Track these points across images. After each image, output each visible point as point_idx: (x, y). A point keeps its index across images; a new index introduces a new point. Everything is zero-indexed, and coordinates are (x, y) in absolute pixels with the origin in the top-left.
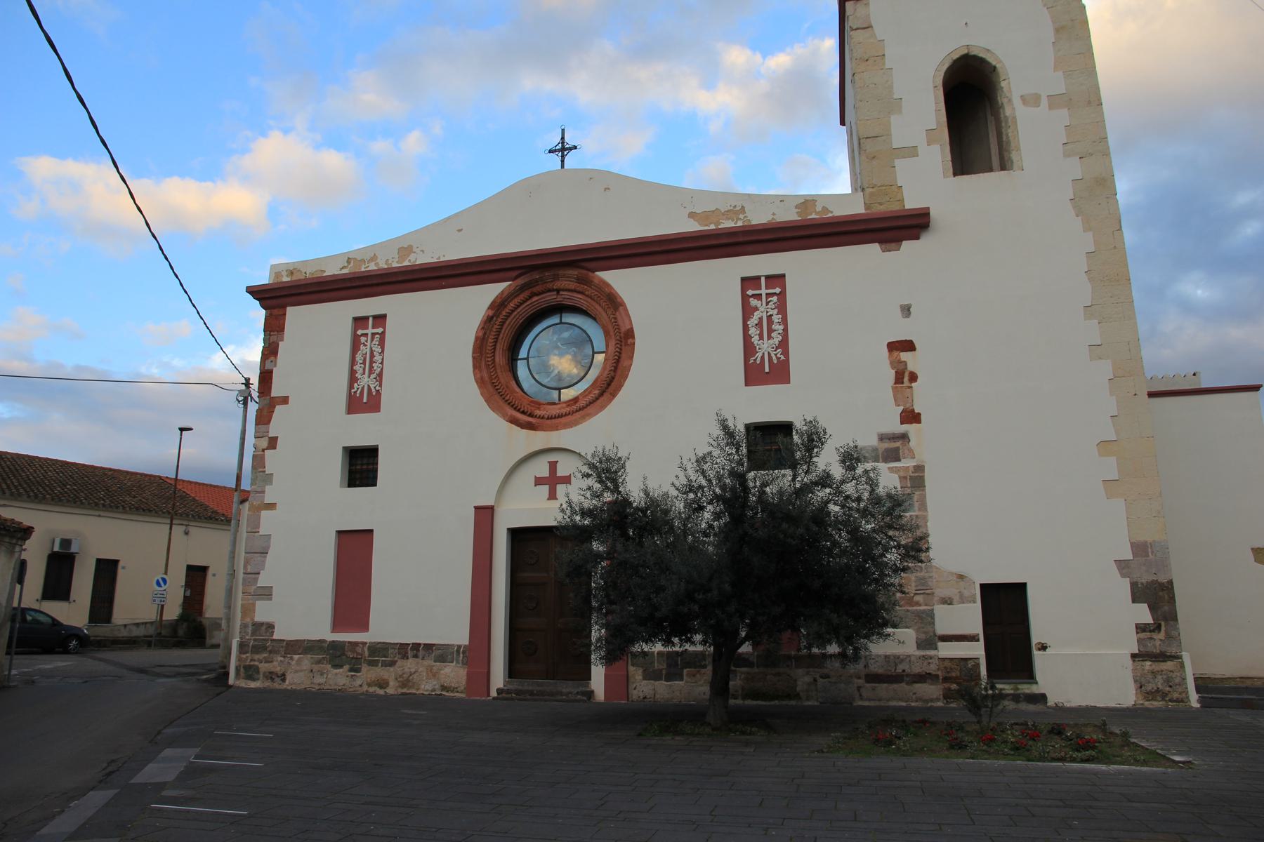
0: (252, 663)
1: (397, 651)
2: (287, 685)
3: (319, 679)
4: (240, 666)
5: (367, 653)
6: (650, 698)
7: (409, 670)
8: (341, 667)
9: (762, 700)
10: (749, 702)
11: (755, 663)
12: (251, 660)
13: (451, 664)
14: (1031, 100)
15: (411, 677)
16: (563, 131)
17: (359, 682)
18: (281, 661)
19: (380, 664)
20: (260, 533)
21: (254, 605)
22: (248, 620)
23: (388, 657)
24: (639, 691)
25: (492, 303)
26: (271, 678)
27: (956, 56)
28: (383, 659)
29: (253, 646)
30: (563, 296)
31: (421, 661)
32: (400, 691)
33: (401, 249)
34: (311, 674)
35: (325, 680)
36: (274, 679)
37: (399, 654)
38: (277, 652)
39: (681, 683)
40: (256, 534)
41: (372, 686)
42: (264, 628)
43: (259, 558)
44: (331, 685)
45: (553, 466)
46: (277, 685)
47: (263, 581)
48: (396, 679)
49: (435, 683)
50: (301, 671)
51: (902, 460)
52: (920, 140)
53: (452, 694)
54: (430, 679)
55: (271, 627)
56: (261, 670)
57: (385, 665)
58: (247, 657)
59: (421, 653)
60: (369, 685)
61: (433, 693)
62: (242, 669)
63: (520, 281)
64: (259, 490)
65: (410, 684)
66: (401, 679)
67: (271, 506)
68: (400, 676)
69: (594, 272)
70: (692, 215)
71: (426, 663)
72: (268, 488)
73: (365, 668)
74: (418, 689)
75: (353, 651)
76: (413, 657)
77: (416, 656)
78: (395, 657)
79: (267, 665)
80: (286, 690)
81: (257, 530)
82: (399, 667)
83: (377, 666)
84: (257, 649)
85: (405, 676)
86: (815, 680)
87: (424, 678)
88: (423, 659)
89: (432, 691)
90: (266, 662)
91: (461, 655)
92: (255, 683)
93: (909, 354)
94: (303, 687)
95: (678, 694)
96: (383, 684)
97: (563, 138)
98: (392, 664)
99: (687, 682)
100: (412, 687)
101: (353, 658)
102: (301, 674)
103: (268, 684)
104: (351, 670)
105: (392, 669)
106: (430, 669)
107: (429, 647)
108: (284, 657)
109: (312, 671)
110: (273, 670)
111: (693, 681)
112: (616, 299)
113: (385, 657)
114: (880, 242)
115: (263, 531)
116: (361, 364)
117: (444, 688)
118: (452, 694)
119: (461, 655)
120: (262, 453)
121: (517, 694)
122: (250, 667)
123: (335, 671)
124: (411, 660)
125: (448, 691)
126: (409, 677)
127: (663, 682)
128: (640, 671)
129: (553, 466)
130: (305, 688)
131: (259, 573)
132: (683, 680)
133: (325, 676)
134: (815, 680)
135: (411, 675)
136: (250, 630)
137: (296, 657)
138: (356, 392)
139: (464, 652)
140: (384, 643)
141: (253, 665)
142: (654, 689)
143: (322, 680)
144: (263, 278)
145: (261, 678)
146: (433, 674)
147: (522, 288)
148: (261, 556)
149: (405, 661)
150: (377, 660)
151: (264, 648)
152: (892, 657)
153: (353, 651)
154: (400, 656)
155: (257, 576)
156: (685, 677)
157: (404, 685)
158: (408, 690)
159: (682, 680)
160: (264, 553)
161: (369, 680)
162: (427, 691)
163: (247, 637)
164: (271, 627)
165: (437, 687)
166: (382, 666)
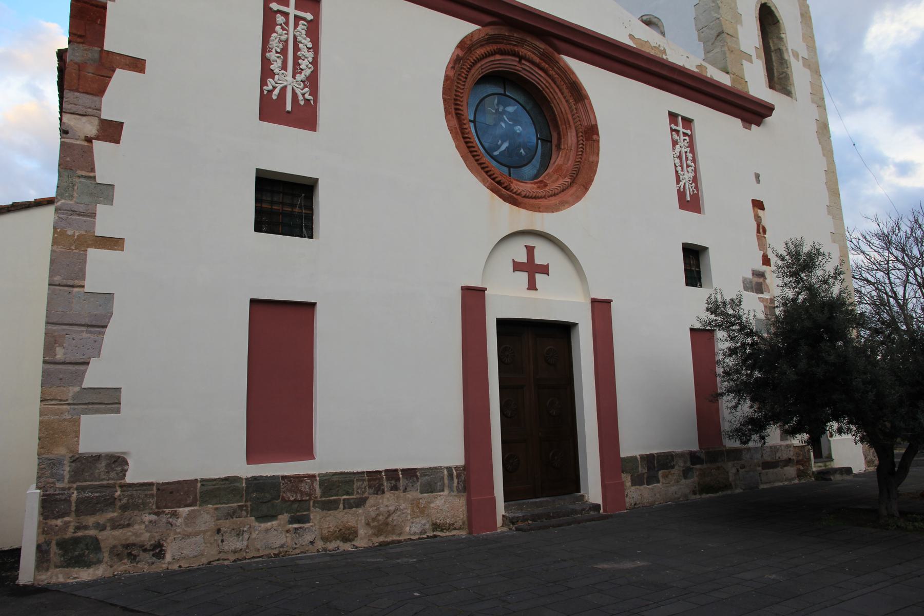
0: (80, 534)
1: (366, 483)
2: (169, 563)
3: (233, 544)
4: (48, 544)
5: (318, 492)
6: (639, 504)
7: (386, 509)
8: (273, 517)
9: (712, 493)
10: (704, 496)
11: (704, 459)
12: (78, 528)
13: (442, 493)
15: (390, 519)
17: (308, 537)
18: (151, 522)
19: (341, 506)
20: (86, 290)
21: (76, 423)
22: (61, 451)
23: (352, 494)
24: (630, 498)
25: (460, 42)
26: (130, 554)
27: (773, 9)
28: (345, 497)
29: (80, 502)
30: (523, 66)
31: (402, 494)
32: (377, 540)
34: (218, 537)
35: (245, 543)
36: (135, 556)
37: (370, 487)
38: (140, 507)
39: (659, 485)
40: (76, 290)
41: (331, 542)
42: (103, 464)
43: (85, 335)
44: (258, 550)
45: (530, 250)
46: (146, 566)
47: (95, 376)
48: (368, 524)
49: (423, 522)
50: (197, 534)
51: (765, 293)
53: (448, 534)
54: (418, 517)
55: (118, 462)
56: (102, 545)
57: (349, 505)
58: (67, 523)
59: (402, 483)
60: (325, 539)
61: (425, 536)
62: (54, 548)
63: (490, 31)
64: (81, 208)
65: (389, 528)
66: (375, 523)
67: (114, 243)
68: (374, 519)
69: (559, 53)
70: (631, 37)
71: (411, 495)
72: (101, 209)
73: (316, 515)
74: (400, 534)
75: (296, 490)
76: (391, 490)
77: (395, 488)
78: (364, 492)
79: (116, 533)
80: (169, 574)
81: (81, 283)
82: (371, 506)
83: (337, 508)
84: (87, 507)
85: (381, 518)
86: (738, 471)
87: (409, 517)
88: (405, 490)
89: (421, 533)
90: (114, 528)
91: (456, 480)
92: (91, 570)
93: (762, 211)
94: (204, 560)
95: (659, 497)
96: (348, 535)
98: (361, 503)
99: (663, 483)
100: (393, 532)
101: (295, 500)
102: (199, 539)
103: (123, 567)
104: (293, 520)
105: (360, 511)
106: (415, 503)
107: (410, 473)
108: (157, 514)
109: (219, 531)
110: (132, 539)
111: (667, 482)
112: (582, 90)
113: (348, 494)
114: (743, 120)
115: (92, 284)
116: (277, 52)
117: (436, 526)
118: (448, 534)
119: (456, 480)
120: (86, 144)
121: (533, 520)
122: (76, 541)
123: (264, 526)
124: (388, 495)
125: (442, 530)
126: (387, 518)
127: (645, 486)
128: (629, 478)
129: (530, 250)
130: (209, 563)
131: (88, 363)
132: (659, 483)
133: (246, 536)
134: (738, 471)
135: (389, 515)
136: (66, 470)
137: (184, 511)
138: (270, 92)
139: (458, 476)
140: (341, 473)
141: (85, 537)
142: (641, 494)
143: (240, 544)
145: (105, 560)
146: (420, 510)
147: (490, 40)
148: (87, 332)
149: (379, 497)
150: (335, 500)
151: (110, 502)
152: (773, 448)
153: (296, 490)
154: (371, 491)
155: (82, 368)
156: (661, 479)
157: (379, 531)
158: (386, 537)
159: (658, 482)
160: (99, 325)
161: (325, 532)
162: (415, 533)
163: (59, 485)
164: (118, 462)
165: (427, 526)
166: (344, 508)
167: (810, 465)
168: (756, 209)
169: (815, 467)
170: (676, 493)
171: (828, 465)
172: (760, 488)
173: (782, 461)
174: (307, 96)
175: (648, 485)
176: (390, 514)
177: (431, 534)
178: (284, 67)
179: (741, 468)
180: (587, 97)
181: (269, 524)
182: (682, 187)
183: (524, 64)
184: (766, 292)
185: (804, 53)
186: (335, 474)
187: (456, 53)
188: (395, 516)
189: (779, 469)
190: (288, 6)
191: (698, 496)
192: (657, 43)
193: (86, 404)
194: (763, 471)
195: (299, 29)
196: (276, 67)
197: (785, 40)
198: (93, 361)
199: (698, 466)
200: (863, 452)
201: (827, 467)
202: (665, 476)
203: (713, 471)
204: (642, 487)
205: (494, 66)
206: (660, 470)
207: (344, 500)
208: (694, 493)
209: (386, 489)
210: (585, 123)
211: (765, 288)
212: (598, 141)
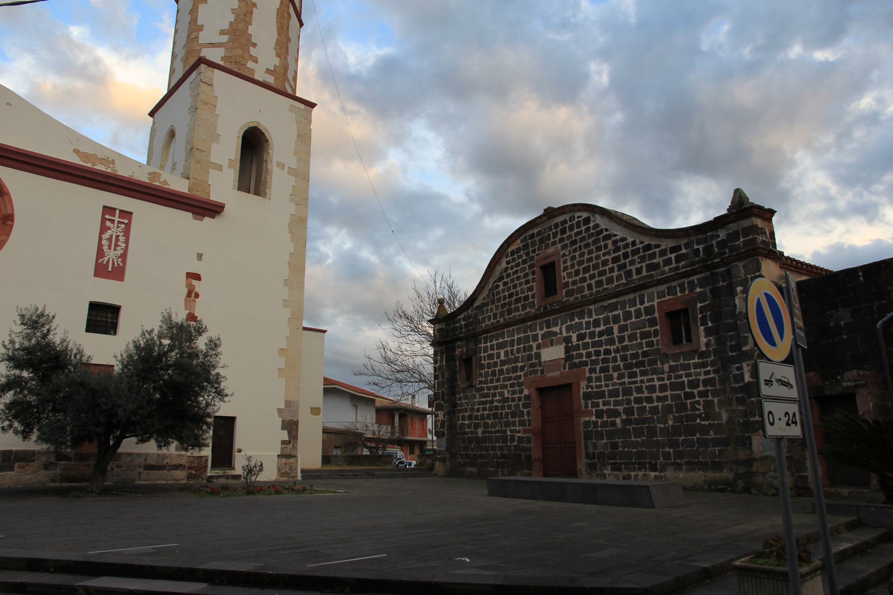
114: (193, 213)
168: (190, 279)
172: (136, 483)
173: (169, 466)
178: (110, 248)
179: (117, 467)
180: (8, 194)
182: (105, 261)
185: (292, 162)
189: (166, 471)
192: (105, 156)
194: (145, 471)
196: (105, 248)
197: (270, 155)
202: (19, 467)
203: (81, 467)
206: (17, 462)
210: (3, 213)
212: (12, 226)
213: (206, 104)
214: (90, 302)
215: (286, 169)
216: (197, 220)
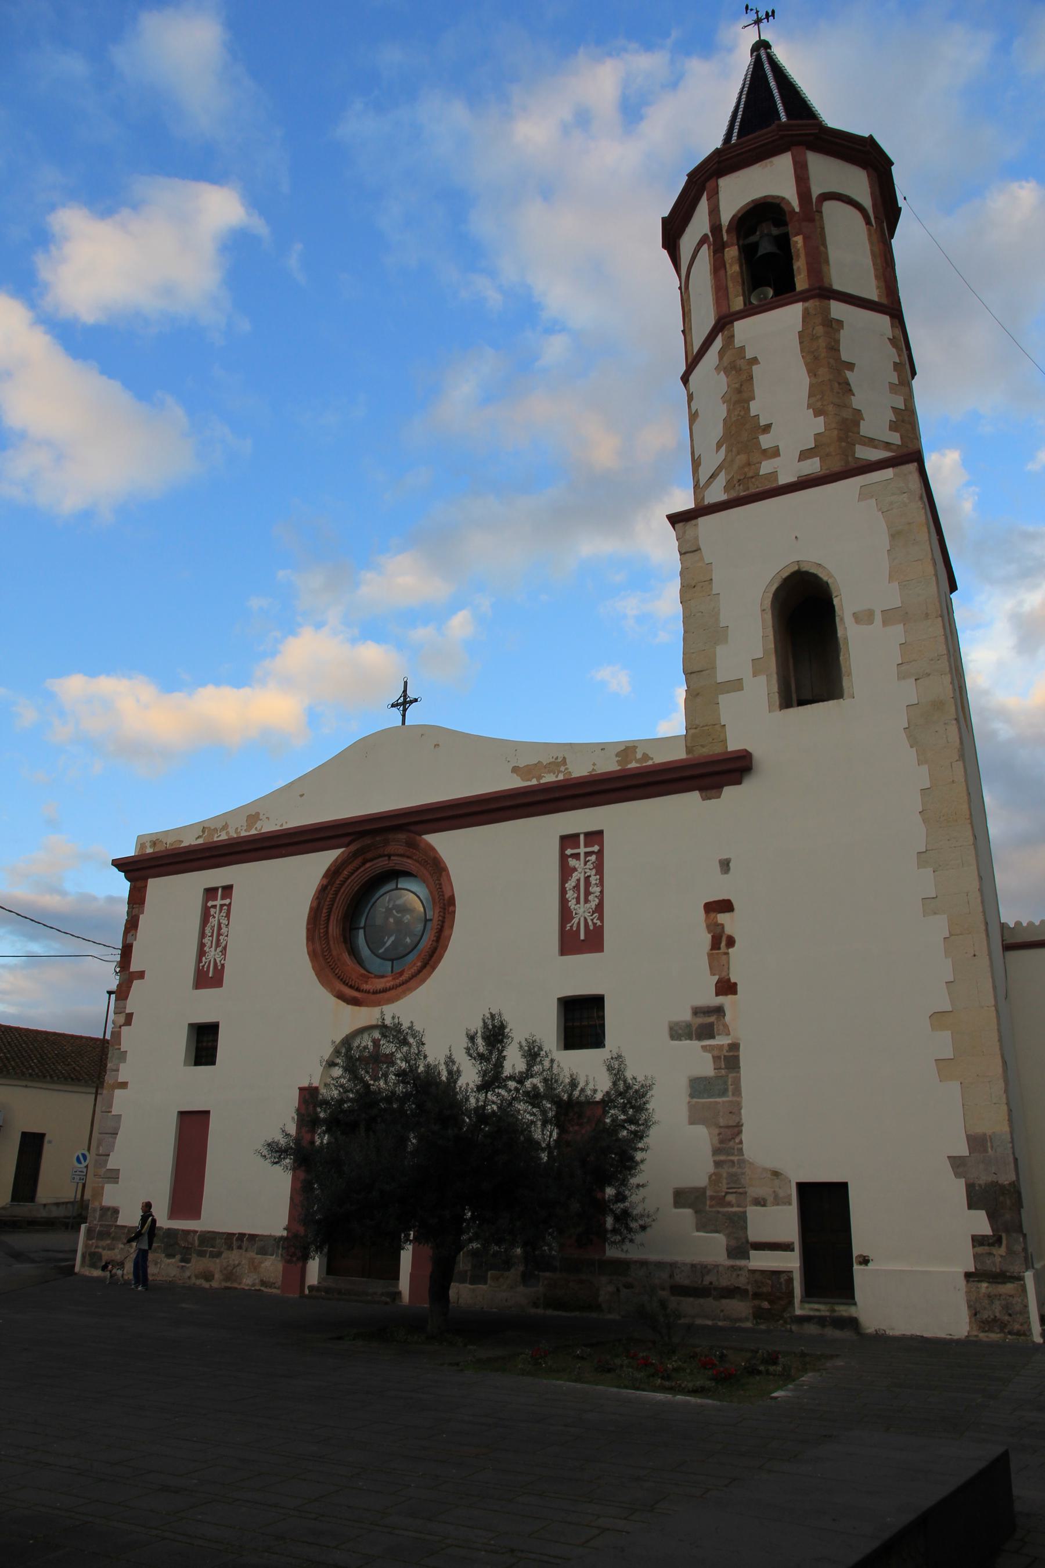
5: (197, 1243)
10: (550, 1312)
14: (864, 617)
15: (234, 1271)
16: (406, 683)
17: (188, 1274)
19: (208, 1255)
20: (113, 1113)
28: (211, 1249)
30: (394, 862)
31: (244, 1253)
32: (224, 1284)
33: (249, 817)
49: (255, 1277)
52: (746, 673)
59: (245, 1243)
60: (197, 1277)
62: (87, 1256)
63: (353, 847)
69: (420, 835)
77: (240, 1247)
79: (109, 1252)
86: (618, 1290)
88: (246, 1251)
96: (208, 1276)
97: (405, 691)
98: (218, 1255)
101: (184, 1247)
104: (182, 1260)
107: (253, 1237)
114: (701, 789)
117: (263, 1283)
124: (235, 1252)
125: (266, 1287)
131: (109, 1155)
134: (618, 1290)
135: (234, 1268)
144: (129, 851)
146: (254, 1267)
147: (355, 855)
151: (108, 1234)
159: (485, 1283)
162: (248, 1285)
164: (115, 1211)
165: (257, 1281)
166: (209, 1257)
167: (791, 1303)
169: (801, 1309)
170: (506, 1300)
171: (828, 1311)
173: (715, 1289)
174: (595, 921)
175: (471, 1283)
176: (235, 1267)
177: (257, 1288)
181: (171, 1260)
182: (575, 925)
183: (394, 860)
184: (719, 1034)
186: (209, 1232)
187: (322, 883)
188: (238, 1268)
190: (586, 846)
191: (540, 1311)
193: (108, 1178)
195: (222, 914)
198: (111, 1154)
199: (548, 1274)
200: (968, 1302)
201: (836, 1314)
204: (461, 1286)
205: (368, 874)
207: (210, 1251)
208: (535, 1305)
209: (234, 1247)
211: (718, 1030)
212: (454, 912)
213: (694, 587)
214: (667, 516)
215: (878, 618)
216: (710, 799)
